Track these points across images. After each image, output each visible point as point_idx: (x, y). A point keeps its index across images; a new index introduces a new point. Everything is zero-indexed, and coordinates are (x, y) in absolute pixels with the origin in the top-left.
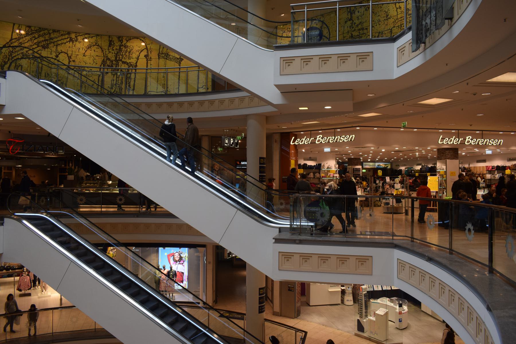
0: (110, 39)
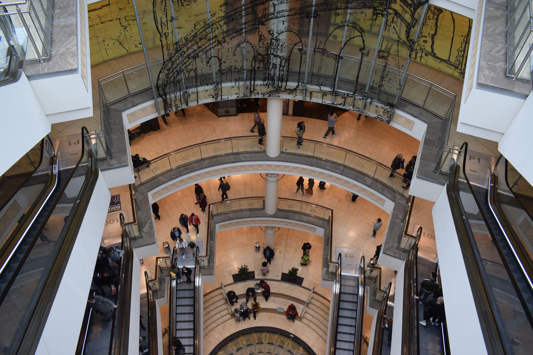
0: (260, 34)
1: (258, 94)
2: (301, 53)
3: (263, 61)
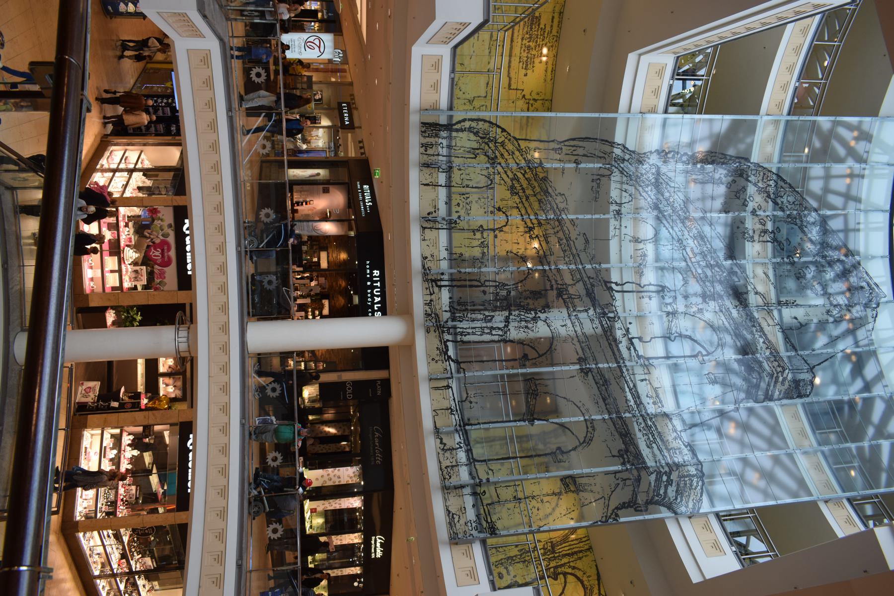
1: (431, 294)
3: (496, 300)
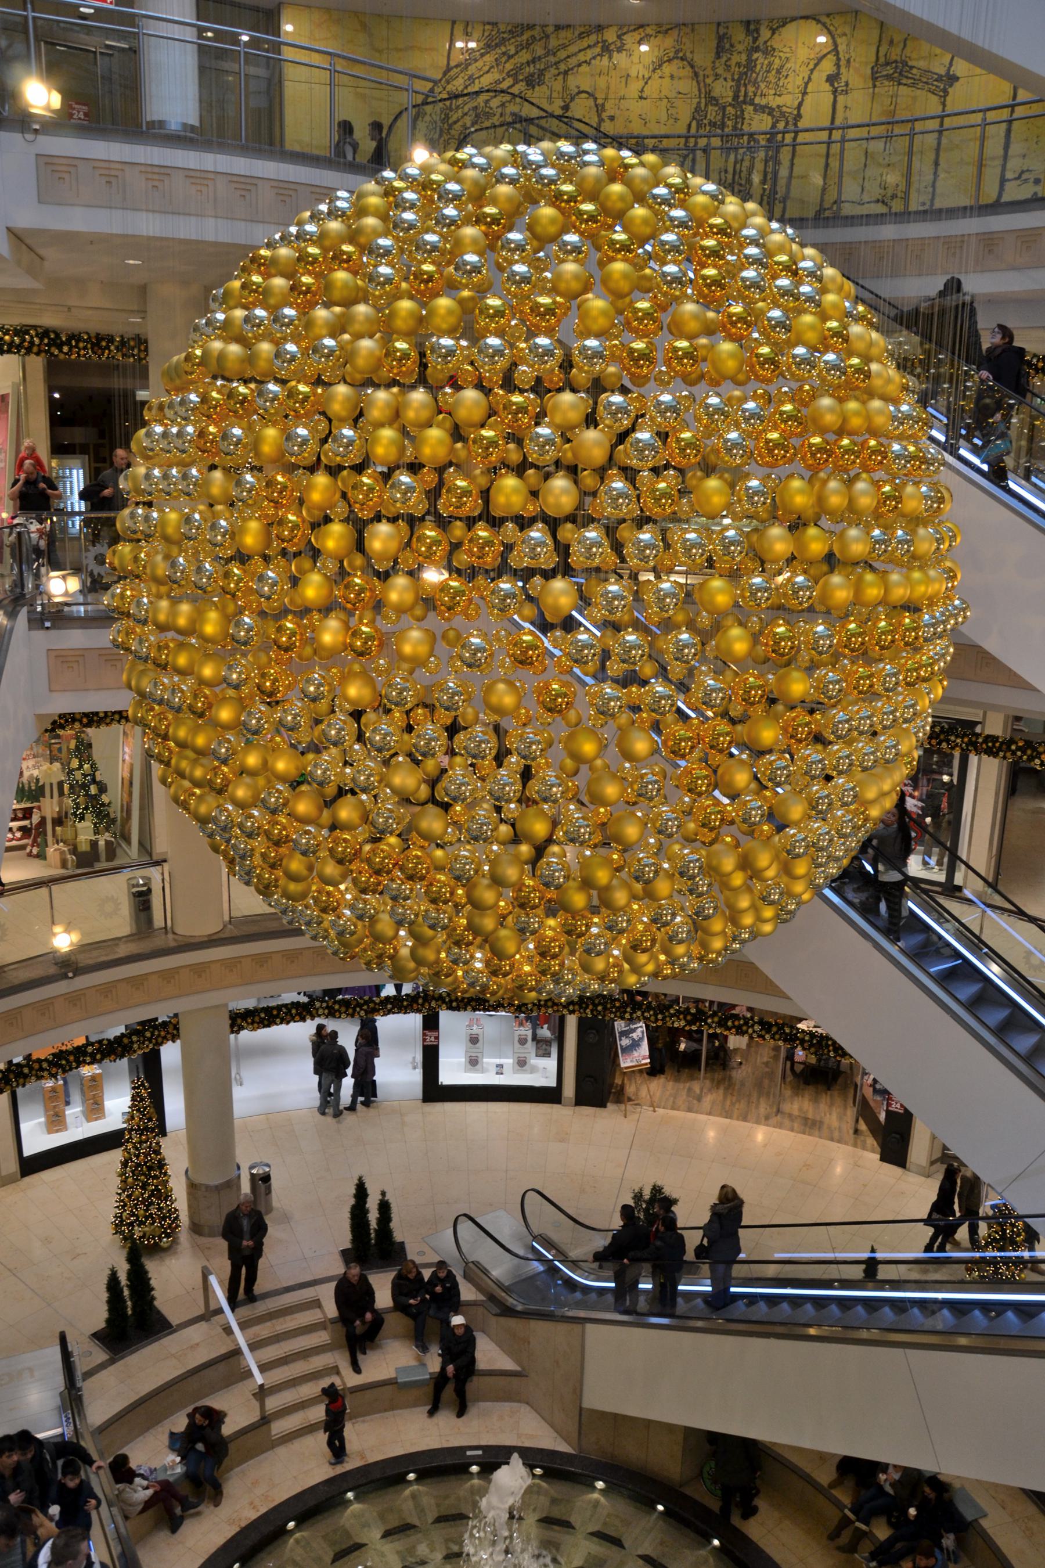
2: (835, 92)
